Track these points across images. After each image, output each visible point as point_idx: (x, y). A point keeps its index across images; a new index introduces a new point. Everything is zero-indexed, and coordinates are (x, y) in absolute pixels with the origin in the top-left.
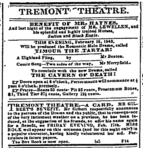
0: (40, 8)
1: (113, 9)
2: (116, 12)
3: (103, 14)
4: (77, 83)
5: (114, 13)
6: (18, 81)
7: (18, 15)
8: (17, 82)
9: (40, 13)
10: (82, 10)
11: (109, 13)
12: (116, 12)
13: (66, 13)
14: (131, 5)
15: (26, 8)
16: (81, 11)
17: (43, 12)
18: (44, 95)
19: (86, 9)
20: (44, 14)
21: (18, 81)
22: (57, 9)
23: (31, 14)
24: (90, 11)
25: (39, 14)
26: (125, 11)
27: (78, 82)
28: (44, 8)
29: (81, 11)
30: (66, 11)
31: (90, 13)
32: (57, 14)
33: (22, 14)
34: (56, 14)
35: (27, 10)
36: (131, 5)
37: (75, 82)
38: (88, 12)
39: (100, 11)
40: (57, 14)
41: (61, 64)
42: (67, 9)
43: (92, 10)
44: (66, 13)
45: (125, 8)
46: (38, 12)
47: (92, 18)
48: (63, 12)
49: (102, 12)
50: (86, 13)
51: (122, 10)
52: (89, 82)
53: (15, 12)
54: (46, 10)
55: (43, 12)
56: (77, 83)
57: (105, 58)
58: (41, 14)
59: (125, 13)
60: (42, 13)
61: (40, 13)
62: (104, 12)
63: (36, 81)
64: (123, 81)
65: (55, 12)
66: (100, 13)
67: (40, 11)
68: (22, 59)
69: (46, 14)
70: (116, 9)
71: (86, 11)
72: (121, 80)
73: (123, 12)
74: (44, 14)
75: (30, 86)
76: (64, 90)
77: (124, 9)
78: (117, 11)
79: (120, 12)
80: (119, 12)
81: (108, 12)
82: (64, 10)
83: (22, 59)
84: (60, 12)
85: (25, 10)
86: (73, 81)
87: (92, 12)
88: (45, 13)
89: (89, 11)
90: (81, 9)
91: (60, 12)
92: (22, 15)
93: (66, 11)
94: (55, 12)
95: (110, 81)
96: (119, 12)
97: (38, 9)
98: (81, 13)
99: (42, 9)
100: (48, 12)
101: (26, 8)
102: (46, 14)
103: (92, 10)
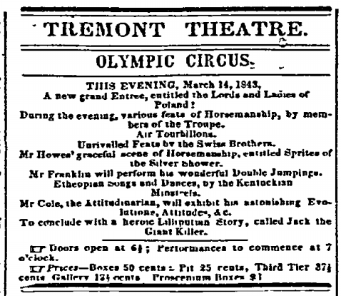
0: (94, 20)
1: (269, 25)
2: (68, 32)
3: (247, 36)
4: (172, 251)
5: (64, 34)
6: (44, 247)
7: (41, 36)
8: (42, 248)
9: (95, 33)
10: (196, 26)
11: (260, 34)
12: (68, 32)
13: (157, 35)
14: (222, 15)
15: (268, 19)
16: (193, 29)
17: (103, 31)
18: (324, 269)
19: (206, 24)
20: (103, 34)
21: (44, 247)
22: (137, 24)
23: (72, 34)
24: (214, 29)
25: (91, 35)
26: (231, 32)
27: (174, 249)
28: (104, 21)
29: (193, 29)
30: (157, 30)
31: (214, 34)
32: (135, 35)
33: (52, 34)
34: (133, 36)
35: (273, 23)
36: (222, 15)
37: (167, 249)
38: (210, 32)
39: (240, 31)
40: (135, 35)
41: (88, 185)
42: (263, 24)
43: (219, 27)
44: (157, 35)
45: (300, 24)
46: (91, 29)
47: (170, 46)
48: (150, 32)
49: (242, 33)
50: (206, 34)
51: (291, 28)
52: (201, 249)
53: (33, 31)
54: (108, 25)
55: (103, 31)
56: (172, 251)
57: (41, 177)
58: (98, 35)
59: (300, 34)
60: (100, 33)
61: (95, 33)
62: (249, 32)
63: (92, 247)
64: (274, 248)
65: (132, 32)
66: (238, 34)
67: (94, 29)
68: (39, 157)
69: (109, 35)
70: (276, 25)
71: (206, 29)
72: (282, 247)
73: (294, 32)
74: (103, 34)
75: (180, 248)
76: (235, 268)
77: (297, 24)
78: (71, 29)
79: (288, 32)
80: (77, 34)
81: (203, 33)
82: (154, 26)
83: (39, 157)
84: (143, 31)
85: (199, 24)
86: (163, 246)
87: (219, 31)
88: (106, 33)
89: (212, 30)
90: (193, 24)
91: (143, 31)
92: (204, 37)
93: (157, 30)
94: (132, 32)
95: (256, 247)
96: (77, 34)
97: (92, 24)
98: (193, 34)
99: (99, 24)
100: (113, 32)
101: (268, 19)
102: (109, 35)
103: (219, 27)
